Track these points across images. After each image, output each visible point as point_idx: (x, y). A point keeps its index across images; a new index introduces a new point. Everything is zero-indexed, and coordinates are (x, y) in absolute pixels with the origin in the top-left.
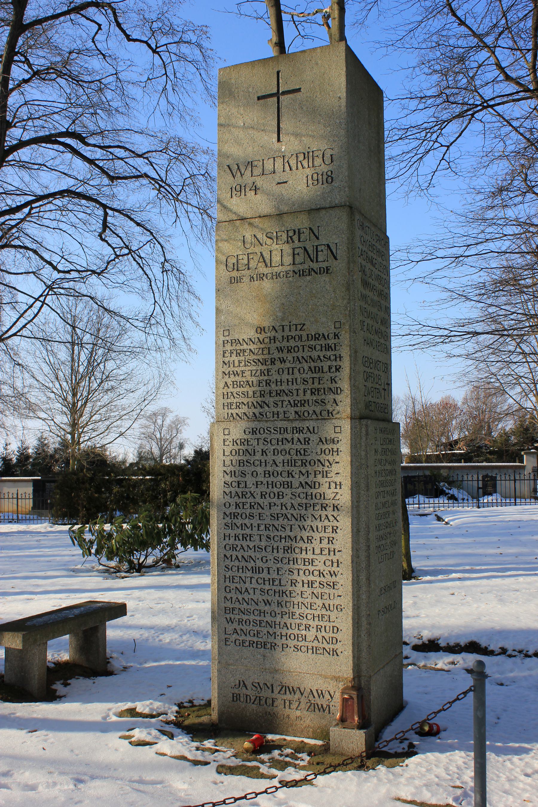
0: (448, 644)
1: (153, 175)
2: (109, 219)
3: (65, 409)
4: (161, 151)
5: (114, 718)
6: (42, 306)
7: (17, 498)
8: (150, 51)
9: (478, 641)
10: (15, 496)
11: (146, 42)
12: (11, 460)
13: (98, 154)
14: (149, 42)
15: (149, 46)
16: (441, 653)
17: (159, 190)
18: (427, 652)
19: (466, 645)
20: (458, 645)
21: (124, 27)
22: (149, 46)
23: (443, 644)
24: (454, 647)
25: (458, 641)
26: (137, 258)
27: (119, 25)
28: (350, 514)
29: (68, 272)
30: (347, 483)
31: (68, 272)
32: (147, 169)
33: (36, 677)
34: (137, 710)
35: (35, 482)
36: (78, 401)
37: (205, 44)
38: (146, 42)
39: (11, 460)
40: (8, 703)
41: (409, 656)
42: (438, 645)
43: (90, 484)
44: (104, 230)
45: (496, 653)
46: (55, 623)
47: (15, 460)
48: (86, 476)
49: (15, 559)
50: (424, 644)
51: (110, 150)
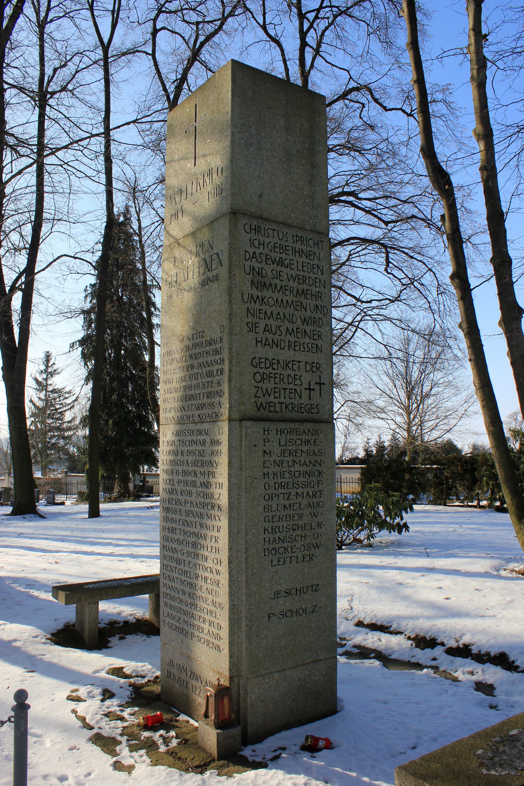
0: (480, 651)
1: (420, 215)
2: (390, 255)
3: (401, 411)
4: (421, 195)
5: (103, 674)
6: (356, 331)
7: (341, 482)
8: (405, 115)
9: (508, 653)
10: (339, 480)
11: (401, 109)
12: (372, 451)
13: (368, 204)
14: (403, 108)
15: (404, 111)
16: (469, 660)
17: (429, 227)
18: (456, 657)
19: (495, 656)
20: (488, 654)
21: (381, 101)
22: (404, 111)
23: (475, 651)
24: (484, 655)
25: (489, 650)
26: (419, 286)
27: (376, 101)
28: (227, 515)
29: (370, 302)
30: (226, 484)
31: (370, 302)
32: (415, 211)
33: (87, 629)
34: (124, 670)
35: (362, 468)
36: (413, 404)
37: (449, 99)
38: (401, 109)
39: (372, 451)
40: (56, 646)
41: (437, 658)
42: (470, 650)
43: (387, 472)
44: (388, 266)
45: (520, 669)
46: (105, 588)
47: (375, 452)
48: (383, 465)
49: (502, 528)
50: (458, 648)
51: (377, 201)
